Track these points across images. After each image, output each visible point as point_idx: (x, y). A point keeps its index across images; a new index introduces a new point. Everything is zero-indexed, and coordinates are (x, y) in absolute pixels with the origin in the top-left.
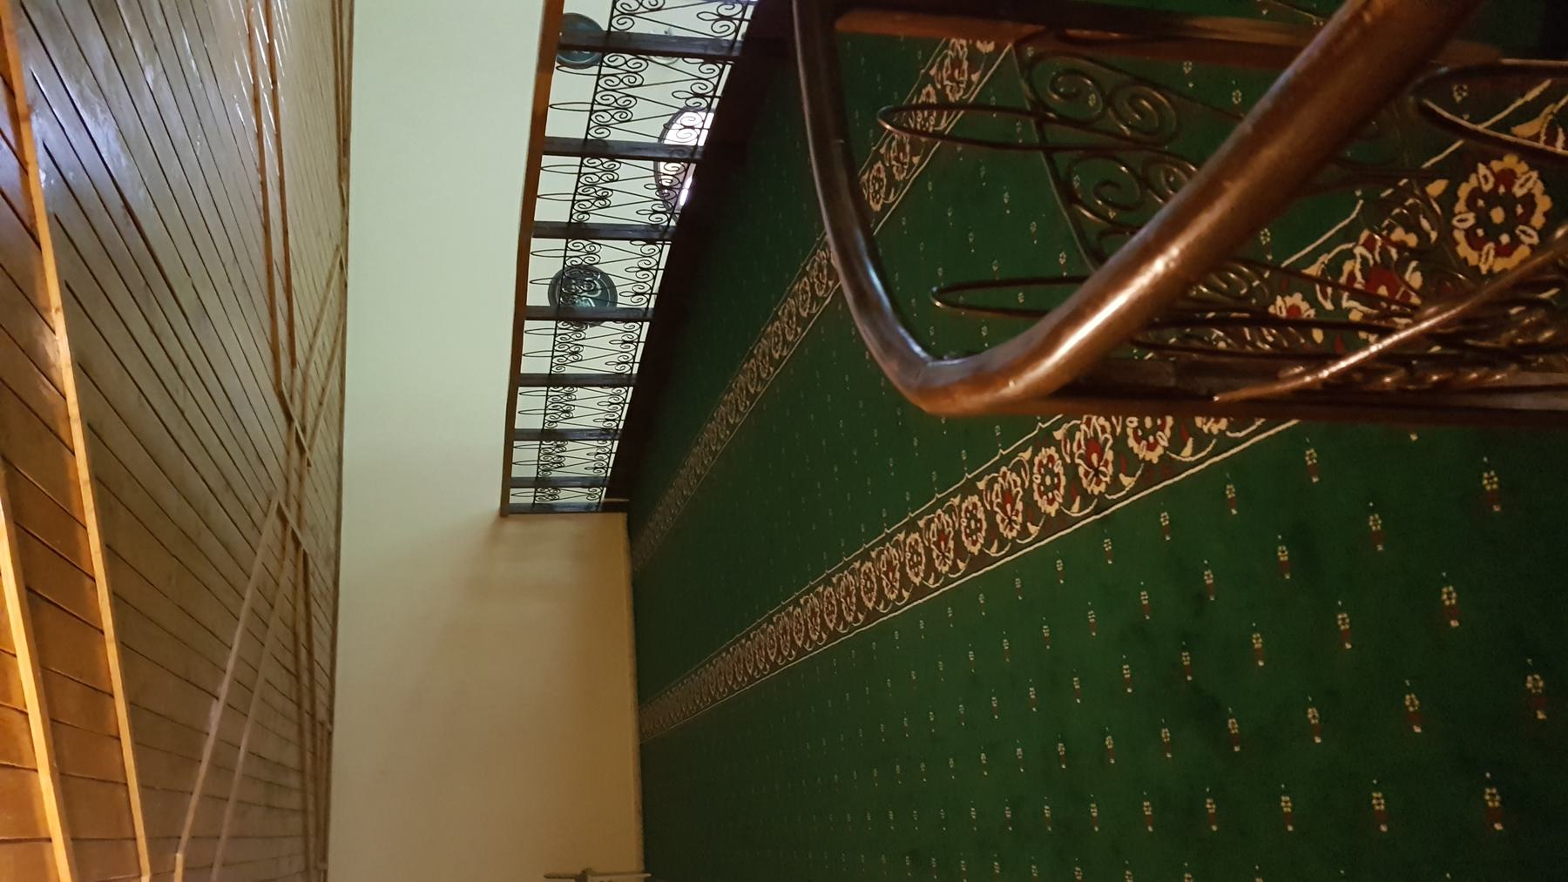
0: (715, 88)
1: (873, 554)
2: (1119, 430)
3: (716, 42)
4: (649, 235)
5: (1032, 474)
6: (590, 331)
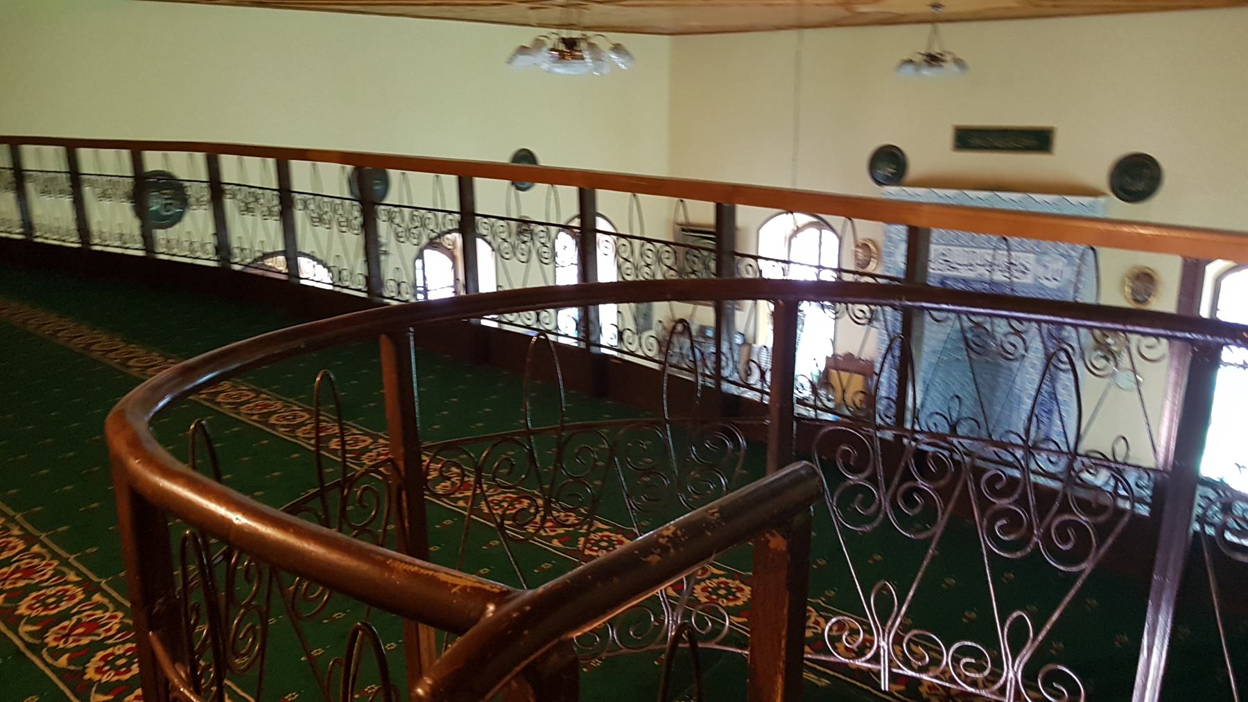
0: (632, 353)
1: (36, 548)
2: (110, 641)
3: (381, 284)
4: (223, 248)
5: (124, 643)
6: (127, 207)
